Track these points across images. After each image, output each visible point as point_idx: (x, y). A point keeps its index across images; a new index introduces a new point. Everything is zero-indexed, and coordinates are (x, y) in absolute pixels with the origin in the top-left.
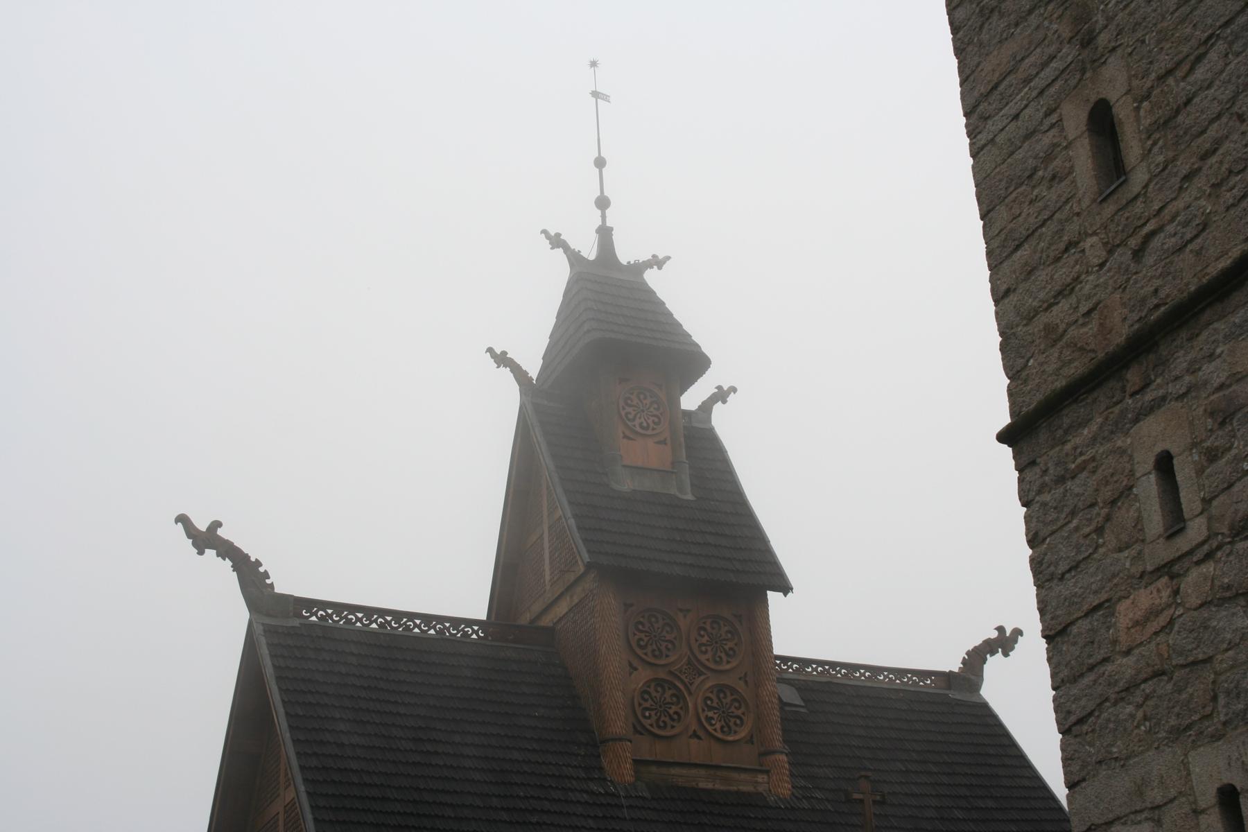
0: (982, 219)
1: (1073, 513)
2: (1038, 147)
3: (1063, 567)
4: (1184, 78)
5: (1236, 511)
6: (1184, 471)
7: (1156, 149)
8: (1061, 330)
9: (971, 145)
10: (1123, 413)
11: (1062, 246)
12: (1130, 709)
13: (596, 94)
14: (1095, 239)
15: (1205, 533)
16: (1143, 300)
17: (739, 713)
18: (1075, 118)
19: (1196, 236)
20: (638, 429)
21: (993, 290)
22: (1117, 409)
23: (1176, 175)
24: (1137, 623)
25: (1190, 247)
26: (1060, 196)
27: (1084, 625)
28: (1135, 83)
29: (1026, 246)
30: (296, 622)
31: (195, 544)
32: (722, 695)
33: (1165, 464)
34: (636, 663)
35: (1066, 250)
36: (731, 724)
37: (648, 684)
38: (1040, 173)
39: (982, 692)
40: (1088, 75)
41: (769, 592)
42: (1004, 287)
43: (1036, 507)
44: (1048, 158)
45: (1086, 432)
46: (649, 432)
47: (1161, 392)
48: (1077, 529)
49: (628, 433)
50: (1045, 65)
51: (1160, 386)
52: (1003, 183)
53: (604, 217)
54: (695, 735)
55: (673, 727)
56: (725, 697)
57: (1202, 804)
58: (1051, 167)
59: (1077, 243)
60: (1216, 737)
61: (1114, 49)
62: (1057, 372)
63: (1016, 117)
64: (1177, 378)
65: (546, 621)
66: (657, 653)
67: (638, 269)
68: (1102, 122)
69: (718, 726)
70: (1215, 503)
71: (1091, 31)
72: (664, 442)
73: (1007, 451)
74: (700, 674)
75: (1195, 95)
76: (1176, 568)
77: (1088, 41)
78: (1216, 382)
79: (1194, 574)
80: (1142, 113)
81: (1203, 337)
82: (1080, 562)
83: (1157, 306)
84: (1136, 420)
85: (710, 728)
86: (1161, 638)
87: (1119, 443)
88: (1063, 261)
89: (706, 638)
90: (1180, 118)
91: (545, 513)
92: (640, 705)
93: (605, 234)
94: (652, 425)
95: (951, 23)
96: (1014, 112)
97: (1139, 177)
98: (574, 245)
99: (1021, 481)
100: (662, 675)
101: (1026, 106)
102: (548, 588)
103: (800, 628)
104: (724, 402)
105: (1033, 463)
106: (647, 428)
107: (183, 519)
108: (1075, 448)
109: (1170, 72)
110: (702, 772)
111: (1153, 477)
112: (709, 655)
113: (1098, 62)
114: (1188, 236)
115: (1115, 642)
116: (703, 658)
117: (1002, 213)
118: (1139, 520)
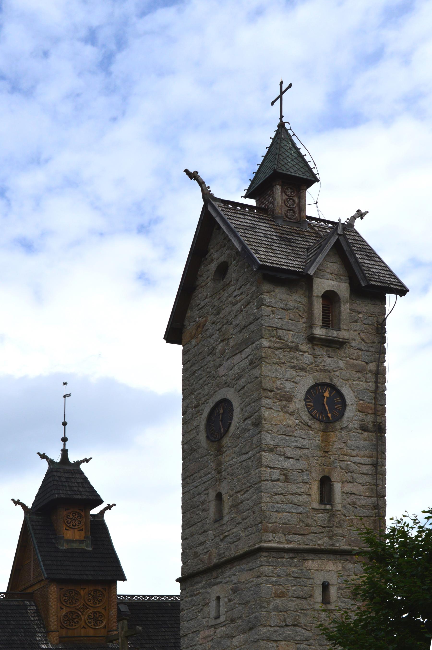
0: (182, 514)
2: (201, 499)
3: (188, 619)
4: (242, 495)
5: (233, 616)
6: (222, 603)
7: (231, 513)
8: (198, 555)
9: (183, 490)
10: (211, 582)
11: (203, 531)
14: (211, 532)
16: (221, 554)
17: (102, 619)
18: (212, 495)
19: (237, 541)
20: (71, 526)
21: (182, 537)
22: (209, 581)
23: (235, 522)
24: (204, 638)
25: (235, 543)
26: (204, 516)
27: (191, 635)
28: (230, 491)
29: (193, 527)
32: (95, 614)
34: (63, 607)
35: (204, 532)
36: (98, 623)
37: (67, 613)
38: (200, 507)
40: (218, 483)
41: (387, 295)
42: (185, 537)
44: (203, 504)
45: (200, 585)
46: (76, 527)
47: (221, 580)
48: (193, 610)
49: (68, 528)
51: (221, 579)
52: (190, 506)
53: (64, 445)
54: (84, 627)
55: (75, 626)
56: (97, 615)
58: (203, 507)
59: (206, 532)
61: (225, 478)
64: (225, 578)
66: (71, 603)
67: (78, 463)
68: (219, 496)
69: (93, 624)
70: (228, 613)
71: (221, 470)
72: (82, 530)
73: (178, 584)
74: (87, 608)
75: (244, 501)
77: (220, 472)
78: (234, 582)
79: (221, 629)
80: (230, 500)
81: (234, 569)
82: (193, 619)
83: (223, 557)
84: (213, 585)
85: (89, 625)
86: (210, 643)
87: (208, 591)
88: (202, 535)
89: (91, 597)
90: (239, 506)
92: (63, 620)
93: (65, 452)
94: (77, 524)
95: (182, 448)
96: (196, 485)
97: (226, 519)
100: (73, 610)
101: (200, 485)
102: (32, 579)
104: (110, 509)
105: (185, 589)
106: (76, 525)
108: (197, 588)
109: (239, 492)
110: (85, 638)
111: (214, 602)
112: (91, 602)
113: (220, 480)
114: (235, 540)
115: (198, 641)
116: (89, 603)
118: (209, 612)
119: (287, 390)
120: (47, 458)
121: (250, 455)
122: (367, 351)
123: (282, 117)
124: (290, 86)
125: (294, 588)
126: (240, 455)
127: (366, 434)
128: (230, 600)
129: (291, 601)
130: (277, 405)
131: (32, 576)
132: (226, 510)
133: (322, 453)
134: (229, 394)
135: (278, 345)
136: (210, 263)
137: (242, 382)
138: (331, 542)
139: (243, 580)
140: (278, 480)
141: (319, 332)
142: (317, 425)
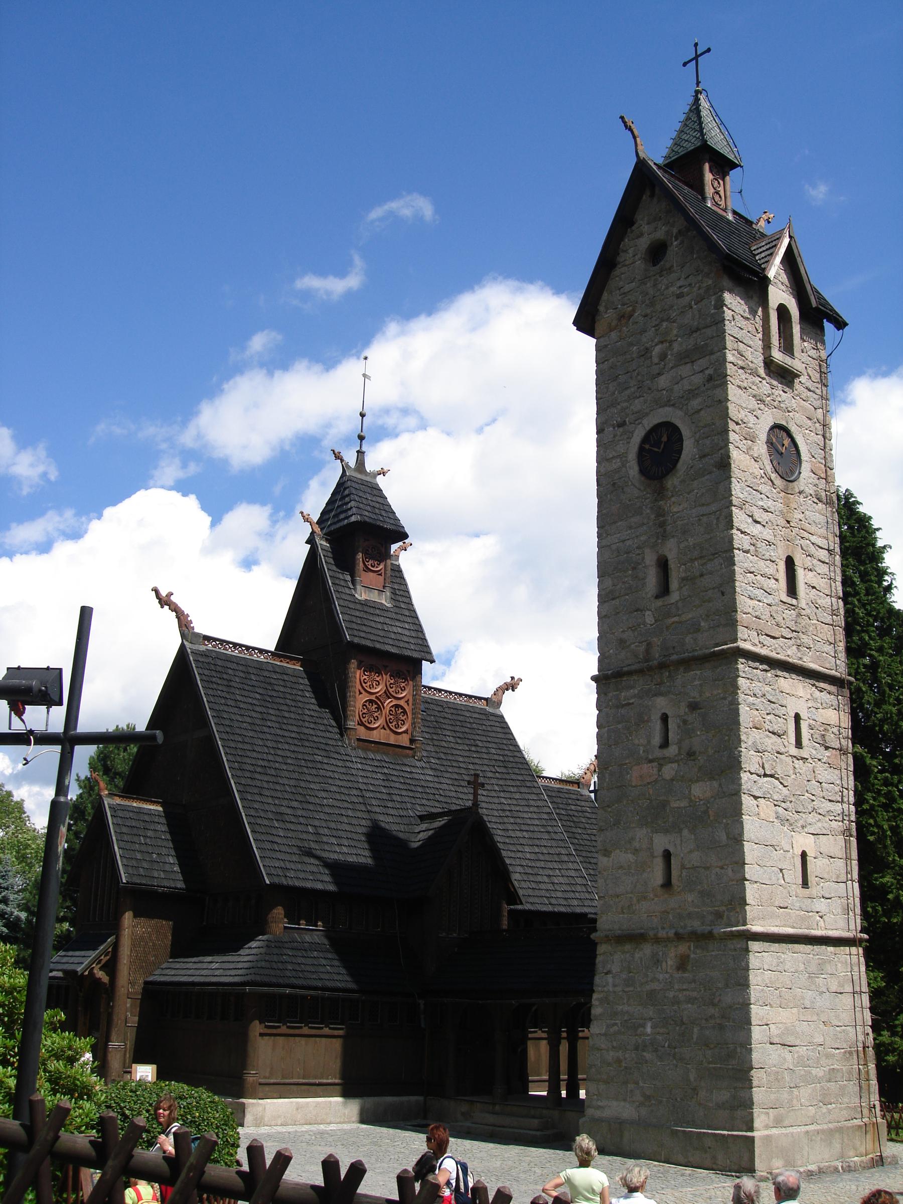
13: (365, 375)
17: (403, 718)
18: (650, 558)
33: (665, 718)
39: (501, 709)
54: (384, 728)
68: (663, 565)
72: (381, 575)
73: (594, 684)
84: (655, 695)
93: (360, 453)
97: (674, 597)
98: (346, 459)
100: (373, 697)
103: (430, 676)
107: (156, 591)
109: (696, 559)
111: (659, 722)
113: (665, 536)
116: (391, 690)
119: (751, 425)
120: (342, 460)
121: (713, 508)
122: (814, 392)
123: (698, 83)
125: (769, 717)
127: (820, 504)
128: (685, 722)
129: (768, 736)
132: (674, 584)
133: (784, 523)
135: (740, 363)
136: (638, 237)
137: (695, 403)
138: (799, 655)
140: (747, 552)
141: (777, 355)
142: (778, 482)
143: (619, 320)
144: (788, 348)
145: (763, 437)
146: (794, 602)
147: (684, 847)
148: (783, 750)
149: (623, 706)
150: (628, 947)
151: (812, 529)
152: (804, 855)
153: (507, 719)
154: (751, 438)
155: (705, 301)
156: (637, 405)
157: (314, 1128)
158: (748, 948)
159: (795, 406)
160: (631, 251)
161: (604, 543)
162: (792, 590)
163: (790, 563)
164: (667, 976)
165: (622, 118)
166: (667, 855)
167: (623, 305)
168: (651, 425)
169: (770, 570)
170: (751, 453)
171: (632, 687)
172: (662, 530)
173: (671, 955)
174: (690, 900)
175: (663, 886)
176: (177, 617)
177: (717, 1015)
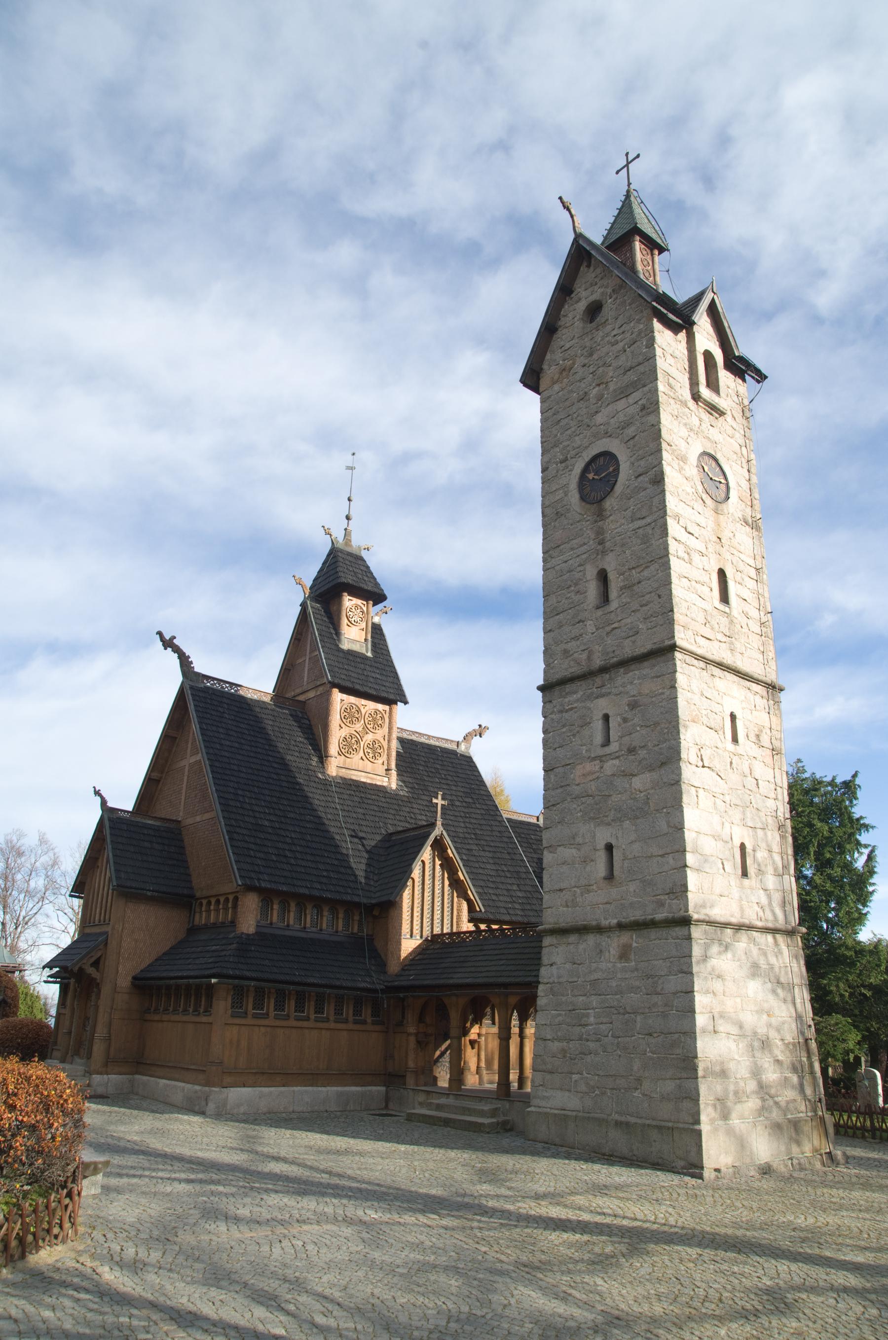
1: (564, 726)
3: (556, 745)
10: (592, 693)
12: (575, 806)
15: (617, 749)
18: (591, 572)
30: (202, 686)
31: (164, 645)
33: (606, 718)
34: (343, 725)
40: (599, 557)
43: (549, 719)
50: (581, 546)
54: (362, 758)
57: (598, 848)
60: (609, 824)
62: (566, 669)
63: (566, 562)
65: (301, 698)
68: (603, 577)
69: (371, 755)
71: (603, 539)
73: (540, 694)
76: (604, 759)
78: (632, 694)
79: (611, 762)
84: (597, 698)
91: (308, 652)
96: (565, 559)
97: (614, 605)
99: (544, 707)
107: (160, 634)
109: (633, 568)
111: (600, 722)
113: (604, 552)
116: (369, 726)
117: (553, 599)
121: (648, 520)
123: (629, 184)
124: (638, 156)
126: (632, 521)
128: (625, 720)
130: (675, 464)
131: (305, 679)
132: (613, 594)
134: (614, 446)
135: (672, 394)
137: (630, 431)
139: (647, 692)
143: (561, 373)
144: (713, 384)
145: (693, 458)
146: (727, 610)
147: (624, 837)
148: (720, 745)
149: (567, 711)
150: (573, 938)
151: (742, 549)
152: (743, 847)
153: (475, 759)
154: (683, 459)
155: (638, 343)
156: (578, 441)
157: (563, 1112)
158: (690, 935)
159: (721, 440)
160: (570, 315)
161: (549, 565)
162: (725, 598)
163: (722, 573)
164: (610, 965)
165: (560, 198)
166: (609, 848)
167: (564, 360)
168: (590, 457)
169: (704, 578)
170: (683, 472)
171: (575, 692)
172: (602, 546)
173: (613, 944)
174: (632, 890)
175: (605, 878)
176: (179, 658)
177: (660, 1003)
